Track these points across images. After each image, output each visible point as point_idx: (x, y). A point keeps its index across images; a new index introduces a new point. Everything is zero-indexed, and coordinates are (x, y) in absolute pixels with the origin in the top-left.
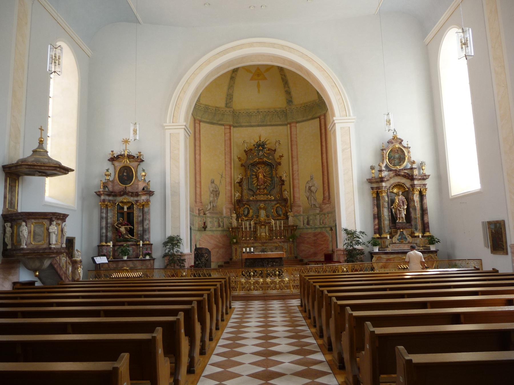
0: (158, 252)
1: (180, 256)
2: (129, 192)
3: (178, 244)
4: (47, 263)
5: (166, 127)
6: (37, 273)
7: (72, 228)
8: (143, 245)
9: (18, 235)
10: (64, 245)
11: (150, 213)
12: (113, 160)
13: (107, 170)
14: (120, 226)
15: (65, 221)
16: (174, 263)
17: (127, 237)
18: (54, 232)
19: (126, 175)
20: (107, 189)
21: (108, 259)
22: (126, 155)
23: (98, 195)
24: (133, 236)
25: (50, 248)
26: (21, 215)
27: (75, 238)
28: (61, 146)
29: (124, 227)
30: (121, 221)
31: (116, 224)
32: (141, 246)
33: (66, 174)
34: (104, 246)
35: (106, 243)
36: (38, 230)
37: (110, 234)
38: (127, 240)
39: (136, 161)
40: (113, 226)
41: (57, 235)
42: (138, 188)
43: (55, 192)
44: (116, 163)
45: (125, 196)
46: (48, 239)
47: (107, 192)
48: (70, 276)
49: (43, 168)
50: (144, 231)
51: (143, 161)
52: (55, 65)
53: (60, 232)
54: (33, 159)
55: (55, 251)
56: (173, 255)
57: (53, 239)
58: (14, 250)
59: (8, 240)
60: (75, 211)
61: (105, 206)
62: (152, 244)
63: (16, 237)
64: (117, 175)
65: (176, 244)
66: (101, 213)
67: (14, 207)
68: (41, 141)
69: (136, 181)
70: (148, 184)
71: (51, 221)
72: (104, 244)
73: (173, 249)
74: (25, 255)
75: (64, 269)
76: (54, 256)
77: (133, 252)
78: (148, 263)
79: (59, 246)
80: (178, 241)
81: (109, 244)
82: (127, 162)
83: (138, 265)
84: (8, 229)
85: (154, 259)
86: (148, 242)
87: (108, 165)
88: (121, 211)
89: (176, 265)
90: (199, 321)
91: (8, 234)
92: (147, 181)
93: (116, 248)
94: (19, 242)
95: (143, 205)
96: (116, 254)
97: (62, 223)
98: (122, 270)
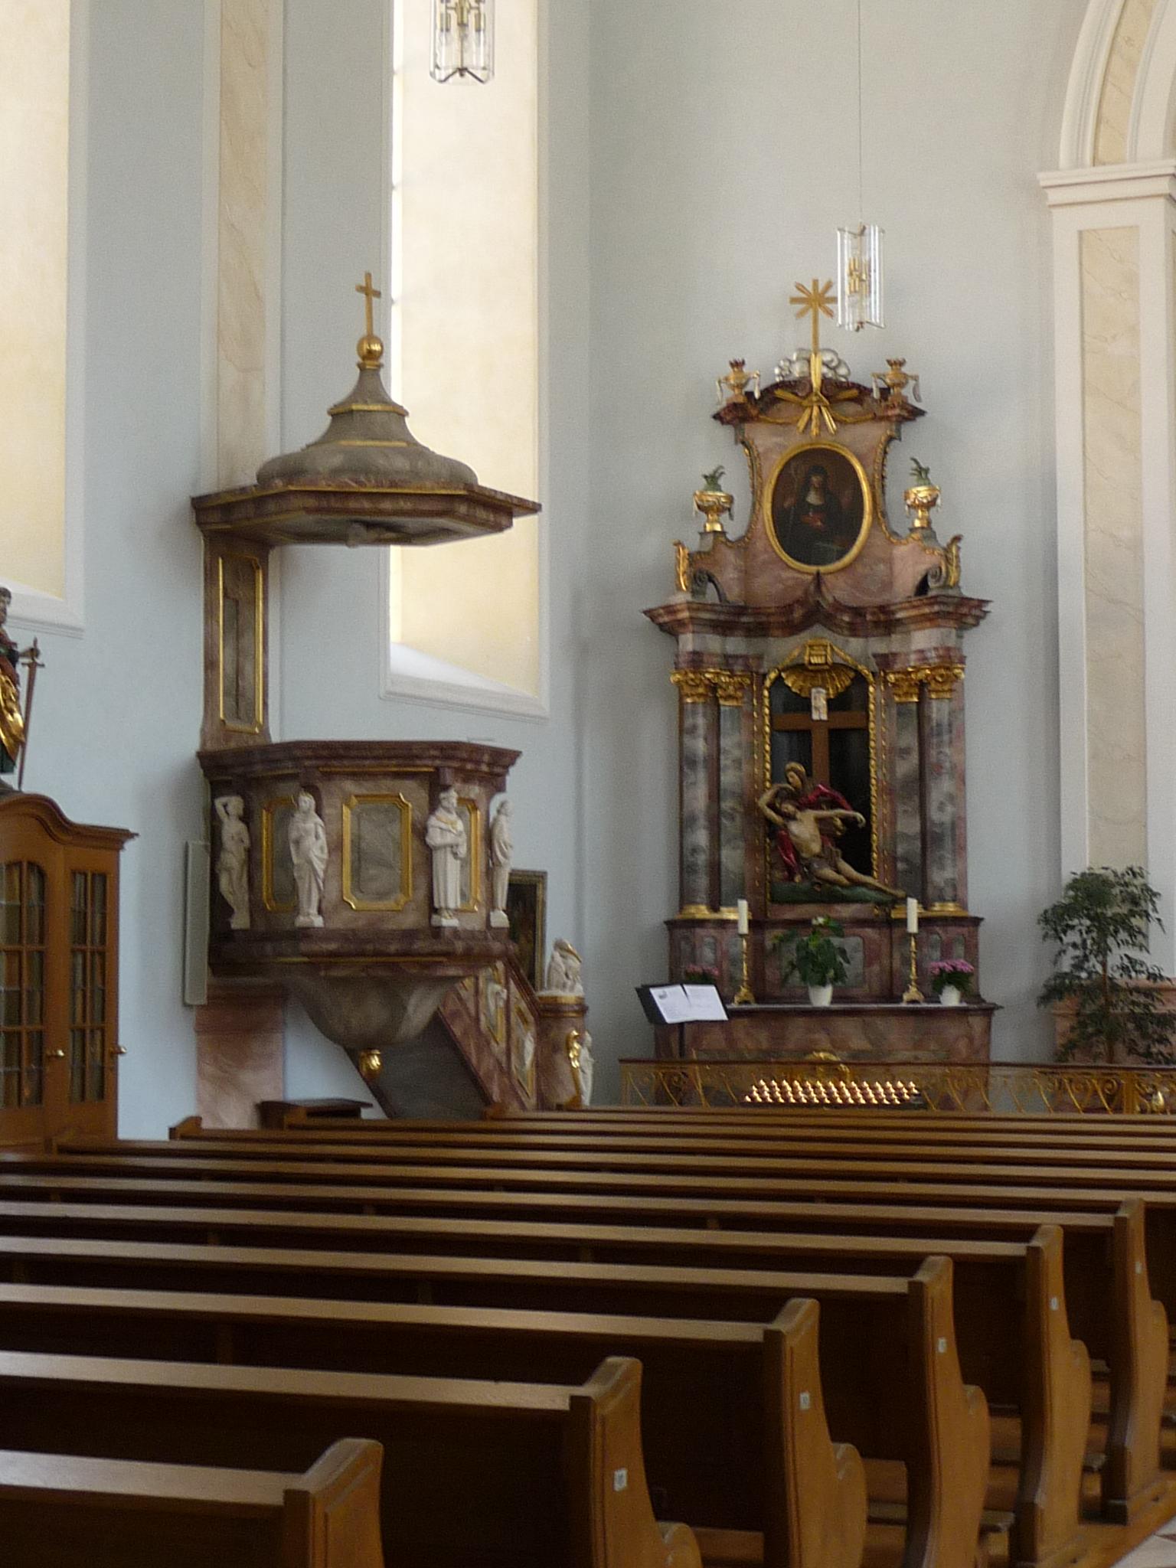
0: (1012, 971)
1: (1147, 993)
2: (839, 607)
3: (1136, 922)
4: (419, 1009)
5: (1054, 196)
6: (375, 1062)
7: (538, 824)
8: (922, 921)
9: (284, 861)
10: (500, 919)
11: (961, 733)
12: (743, 412)
13: (713, 480)
14: (789, 808)
15: (501, 788)
16: (1112, 1039)
17: (829, 873)
18: (453, 848)
19: (819, 504)
20: (711, 595)
21: (725, 1000)
22: (816, 382)
23: (662, 627)
24: (867, 870)
25: (437, 932)
26: (295, 759)
27: (541, 877)
28: (466, 384)
29: (811, 814)
30: (794, 779)
31: (767, 797)
32: (913, 927)
33: (498, 528)
34: (702, 923)
35: (715, 907)
36: (375, 838)
37: (732, 858)
38: (829, 895)
39: (877, 419)
40: (750, 809)
41: (465, 863)
42: (888, 585)
43: (439, 631)
44: (762, 436)
45: (818, 630)
46: (422, 881)
47: (710, 608)
48: (530, 1087)
49: (387, 505)
50: (929, 839)
51: (915, 413)
52: (463, 38)
53: (481, 848)
54: (337, 460)
55: (459, 946)
56: (1105, 987)
57: (451, 882)
58: (266, 937)
59: (233, 886)
60: (539, 720)
61: (701, 692)
62: (976, 921)
63: (272, 867)
64: (767, 506)
65: (1122, 922)
66: (683, 731)
67: (251, 718)
68: (371, 355)
69: (879, 541)
70: (950, 553)
71: (435, 787)
72: (702, 912)
73: (1103, 951)
74: (318, 963)
75: (498, 1048)
76: (452, 972)
77: (868, 962)
78: (953, 1030)
79: (474, 923)
80: (1134, 901)
81: (727, 914)
82: (819, 426)
83: (897, 1036)
84: (233, 829)
85: (988, 1011)
86: (951, 908)
87: (716, 449)
88: (795, 721)
89: (1120, 1049)
90: (1155, 1295)
91: (233, 857)
92: (944, 540)
93: (771, 937)
94: (289, 896)
95: (922, 685)
96: (771, 974)
97: (490, 798)
98: (803, 1066)
